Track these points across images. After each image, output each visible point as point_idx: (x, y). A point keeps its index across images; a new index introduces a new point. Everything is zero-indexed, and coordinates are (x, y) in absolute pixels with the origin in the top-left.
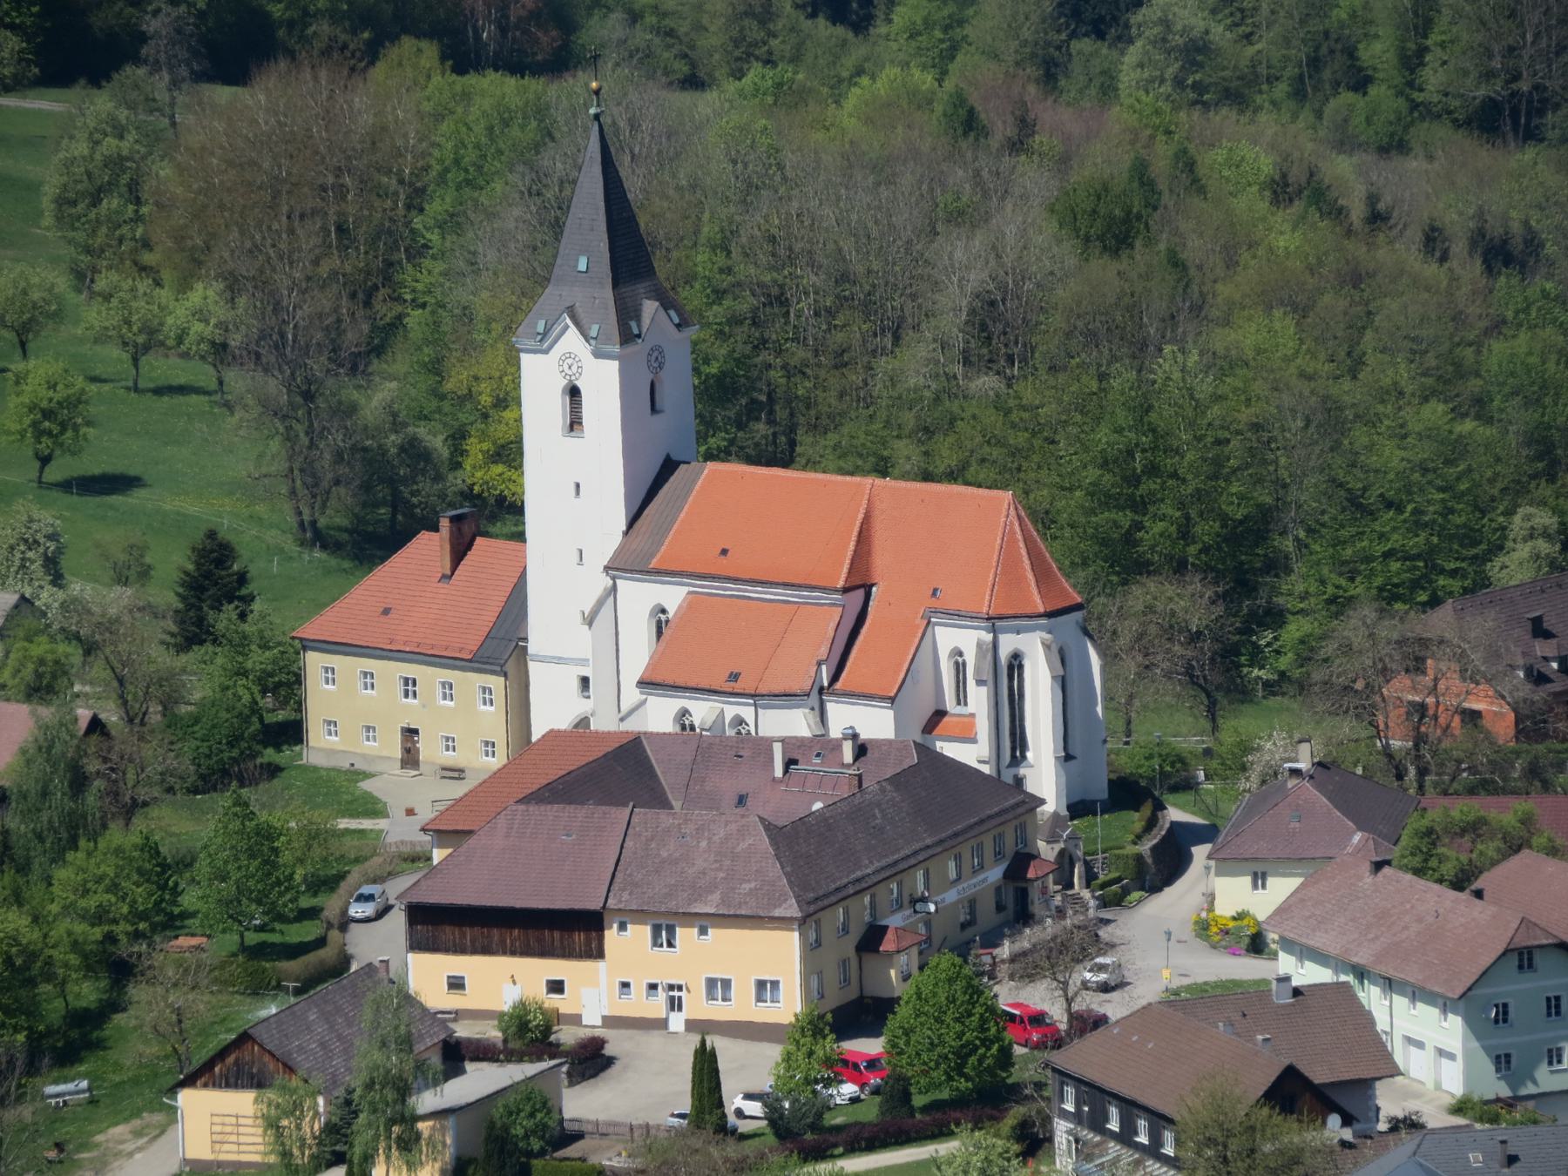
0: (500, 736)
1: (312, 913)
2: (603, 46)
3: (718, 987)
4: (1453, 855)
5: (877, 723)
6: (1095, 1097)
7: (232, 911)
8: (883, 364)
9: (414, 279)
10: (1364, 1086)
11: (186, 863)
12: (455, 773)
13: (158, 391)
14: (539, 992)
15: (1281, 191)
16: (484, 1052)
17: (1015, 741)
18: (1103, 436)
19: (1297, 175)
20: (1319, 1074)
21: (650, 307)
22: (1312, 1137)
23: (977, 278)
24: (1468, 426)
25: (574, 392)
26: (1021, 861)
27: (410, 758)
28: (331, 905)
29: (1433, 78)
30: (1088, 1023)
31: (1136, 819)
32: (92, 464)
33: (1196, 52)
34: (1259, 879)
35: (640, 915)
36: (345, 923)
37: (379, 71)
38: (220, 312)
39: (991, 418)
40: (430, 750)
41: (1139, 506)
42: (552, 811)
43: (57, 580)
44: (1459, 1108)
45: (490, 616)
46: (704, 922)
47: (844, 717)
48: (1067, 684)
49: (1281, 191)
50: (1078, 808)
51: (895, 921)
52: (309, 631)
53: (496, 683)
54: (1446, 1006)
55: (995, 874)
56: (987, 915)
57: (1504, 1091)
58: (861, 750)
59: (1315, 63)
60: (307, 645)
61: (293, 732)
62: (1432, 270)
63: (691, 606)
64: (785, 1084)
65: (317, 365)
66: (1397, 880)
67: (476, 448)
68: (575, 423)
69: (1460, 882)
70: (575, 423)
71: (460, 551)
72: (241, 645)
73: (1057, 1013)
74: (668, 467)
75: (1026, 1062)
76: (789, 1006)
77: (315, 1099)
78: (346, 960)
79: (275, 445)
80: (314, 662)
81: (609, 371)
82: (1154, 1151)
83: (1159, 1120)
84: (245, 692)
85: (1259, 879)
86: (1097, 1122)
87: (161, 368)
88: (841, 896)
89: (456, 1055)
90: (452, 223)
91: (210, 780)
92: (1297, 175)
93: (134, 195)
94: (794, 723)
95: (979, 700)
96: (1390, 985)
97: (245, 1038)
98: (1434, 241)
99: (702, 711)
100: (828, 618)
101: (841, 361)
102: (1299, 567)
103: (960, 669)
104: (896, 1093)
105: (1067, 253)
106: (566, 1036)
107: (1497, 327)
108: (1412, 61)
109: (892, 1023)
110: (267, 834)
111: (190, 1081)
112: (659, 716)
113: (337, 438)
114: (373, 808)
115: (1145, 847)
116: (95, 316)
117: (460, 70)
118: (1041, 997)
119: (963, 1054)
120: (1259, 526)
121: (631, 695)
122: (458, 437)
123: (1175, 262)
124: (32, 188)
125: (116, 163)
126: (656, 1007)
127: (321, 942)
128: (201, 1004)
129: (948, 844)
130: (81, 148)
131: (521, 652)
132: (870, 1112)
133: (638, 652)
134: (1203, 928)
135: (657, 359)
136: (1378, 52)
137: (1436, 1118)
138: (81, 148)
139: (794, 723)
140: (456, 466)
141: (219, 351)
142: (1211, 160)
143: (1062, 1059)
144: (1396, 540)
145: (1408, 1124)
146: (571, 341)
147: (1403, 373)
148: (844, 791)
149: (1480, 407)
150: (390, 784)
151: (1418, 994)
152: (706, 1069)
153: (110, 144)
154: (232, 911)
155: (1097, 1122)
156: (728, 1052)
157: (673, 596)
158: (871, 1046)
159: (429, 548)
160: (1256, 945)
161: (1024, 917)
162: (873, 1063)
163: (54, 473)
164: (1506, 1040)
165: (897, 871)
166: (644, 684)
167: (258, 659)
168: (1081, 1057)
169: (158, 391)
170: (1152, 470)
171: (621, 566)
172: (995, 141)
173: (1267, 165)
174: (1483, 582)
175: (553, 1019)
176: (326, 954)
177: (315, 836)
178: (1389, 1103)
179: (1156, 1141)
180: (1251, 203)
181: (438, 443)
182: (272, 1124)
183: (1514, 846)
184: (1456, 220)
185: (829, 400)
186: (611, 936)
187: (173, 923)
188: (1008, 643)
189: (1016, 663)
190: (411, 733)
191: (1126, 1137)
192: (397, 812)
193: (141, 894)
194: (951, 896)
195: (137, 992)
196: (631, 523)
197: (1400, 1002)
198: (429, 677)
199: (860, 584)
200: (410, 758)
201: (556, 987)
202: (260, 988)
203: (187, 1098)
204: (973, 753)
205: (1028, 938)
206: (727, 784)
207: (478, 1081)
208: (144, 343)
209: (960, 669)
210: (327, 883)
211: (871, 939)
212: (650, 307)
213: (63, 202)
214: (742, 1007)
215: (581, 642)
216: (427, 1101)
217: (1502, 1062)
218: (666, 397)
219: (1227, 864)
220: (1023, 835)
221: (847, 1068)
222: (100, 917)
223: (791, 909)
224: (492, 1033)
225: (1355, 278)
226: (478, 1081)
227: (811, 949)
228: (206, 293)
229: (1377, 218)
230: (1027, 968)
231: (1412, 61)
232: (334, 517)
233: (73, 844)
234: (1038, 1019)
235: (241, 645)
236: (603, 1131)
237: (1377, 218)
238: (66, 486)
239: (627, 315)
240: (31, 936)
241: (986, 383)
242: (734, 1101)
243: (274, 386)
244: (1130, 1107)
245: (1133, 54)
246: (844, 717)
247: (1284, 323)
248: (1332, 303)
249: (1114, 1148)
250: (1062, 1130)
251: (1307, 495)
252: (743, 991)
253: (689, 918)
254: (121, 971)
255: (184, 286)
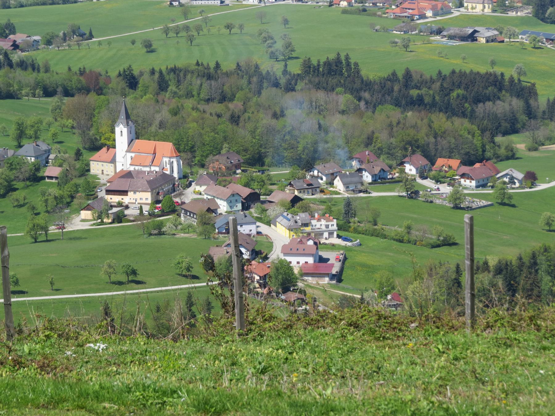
0: (113, 171)
1: (93, 191)
2: (367, 107)
3: (141, 199)
4: (223, 183)
5: (157, 169)
6: (186, 211)
7: (85, 191)
8: (149, 129)
9: (94, 119)
10: (216, 209)
11: (79, 185)
12: (108, 175)
13: (65, 132)
14: (120, 200)
15: (193, 109)
16: (115, 206)
17: (172, 171)
18: (175, 137)
19: (195, 107)
20: (212, 208)
21: (130, 122)
22: (212, 215)
23: (160, 119)
24: (216, 135)
25: (121, 132)
26: (174, 184)
27: (103, 173)
28: (95, 190)
29: (202, 96)
30: (183, 203)
31: (186, 180)
32: (59, 140)
33: (175, 93)
34: (201, 186)
35: (132, 191)
36: (97, 192)
37: (89, 95)
38: (72, 122)
39: (162, 135)
40: (105, 172)
41: (179, 145)
42: (122, 179)
43: (60, 153)
44: (226, 212)
45: (112, 158)
46: (139, 191)
47: (153, 168)
48: (178, 165)
49: (193, 109)
50: (180, 179)
51: (161, 191)
52: (91, 159)
53: (113, 165)
54: (224, 201)
55: (171, 186)
56: (170, 191)
57: (230, 210)
58: (156, 172)
59: (188, 94)
60: (91, 160)
61: (89, 170)
62: (211, 118)
63: (135, 156)
64: (150, 210)
65: (85, 129)
66: (218, 186)
67: (103, 138)
68: (122, 135)
69: (224, 186)
70: (122, 135)
71: (108, 150)
72: (83, 161)
73: (180, 202)
74: (132, 140)
75: (178, 208)
76: (149, 201)
77: (312, 255)
78: (97, 197)
79: (80, 138)
80: (91, 163)
81: (126, 129)
82: (193, 217)
83: (194, 214)
84: (83, 166)
85: (201, 186)
86: (186, 214)
87: (65, 129)
88: (155, 189)
89: (112, 207)
90: (99, 113)
91: (80, 176)
92: (195, 107)
93: (60, 109)
94: (147, 169)
95: (168, 166)
96: (218, 198)
97: (88, 205)
98: (211, 114)
99: (137, 168)
100: (151, 157)
101: (145, 128)
102: (198, 152)
103: (166, 163)
104: (163, 211)
105: (170, 116)
106: (124, 204)
107: (219, 124)
108: (199, 94)
109: (162, 203)
110: (89, 182)
111: (82, 210)
112: (132, 168)
113: (87, 137)
114: (99, 179)
115: (188, 183)
116: (57, 124)
117: (98, 95)
118: (177, 200)
119: (170, 206)
120: (193, 147)
121: (128, 166)
122: (100, 137)
123: (183, 117)
124: (48, 109)
125: (58, 106)
126: (134, 201)
127: (95, 194)
128: (83, 201)
129: (166, 183)
130: (54, 104)
131: (115, 161)
132: (160, 213)
133: (129, 161)
134: (194, 192)
135: (131, 127)
136: (195, 93)
137: (224, 214)
138: (54, 104)
139: (147, 169)
140: (100, 140)
141: (73, 127)
142: (185, 105)
143: (182, 207)
144: (209, 148)
145: (221, 214)
146: (121, 126)
147: (208, 129)
148: (155, 177)
149: (217, 133)
150: (100, 176)
151: (221, 199)
152: (141, 209)
153: (57, 104)
154: (85, 191)
155: (186, 214)
156: (143, 206)
157: (133, 155)
158: (160, 205)
159: (104, 149)
160: (200, 194)
161: (174, 191)
162: (159, 207)
163: (55, 141)
164: (231, 204)
165: (161, 186)
166: (130, 165)
167: (85, 162)
168: (183, 206)
169: (65, 132)
170: (181, 141)
171: (127, 151)
172: (160, 103)
173: (191, 106)
174: (220, 153)
175: (122, 203)
176: (95, 195)
177: (93, 182)
178: (219, 211)
179: (193, 216)
180: (190, 110)
181: (98, 138)
182: (93, 215)
183: (230, 183)
184: (213, 112)
185: (143, 133)
186: (129, 193)
187: (78, 192)
188: (172, 160)
189: (173, 162)
190: (103, 170)
191: (190, 216)
192: (102, 179)
193: (75, 189)
194: (166, 188)
195: (75, 200)
196: (128, 146)
197: (219, 200)
198: (105, 164)
199: (155, 153)
200: (103, 173)
201: (122, 199)
202: (88, 199)
203: (82, 212)
204: (168, 172)
205: (175, 193)
206: (141, 176)
207: (115, 210)
208: (64, 126)
209: (166, 163)
210: (95, 187)
211: (158, 193)
212: (130, 122)
213: (52, 110)
214: (144, 201)
215: (122, 160)
216: (110, 212)
217: (231, 207)
218: (132, 132)
219: (197, 184)
220: (174, 181)
221: (156, 208)
222: (70, 191)
223: (149, 190)
224: (115, 204)
225: (203, 119)
226: (115, 210)
227: (152, 194)
228: (70, 121)
229: (204, 112)
230: (176, 196)
231: (199, 94)
232: (87, 146)
233: (66, 183)
234: (177, 202)
235: (83, 161)
236: (129, 215)
237: (204, 112)
238: (56, 143)
239: (127, 123)
240: (62, 194)
241: (161, 131)
242: (144, 212)
243: (80, 131)
244: (190, 212)
245: (168, 93)
246: (153, 168)
247: (195, 124)
248: (201, 121)
249: (188, 217)
250: (182, 215)
251: (198, 144)
252: (144, 199)
253: (138, 191)
254: (72, 197)
255: (67, 120)
